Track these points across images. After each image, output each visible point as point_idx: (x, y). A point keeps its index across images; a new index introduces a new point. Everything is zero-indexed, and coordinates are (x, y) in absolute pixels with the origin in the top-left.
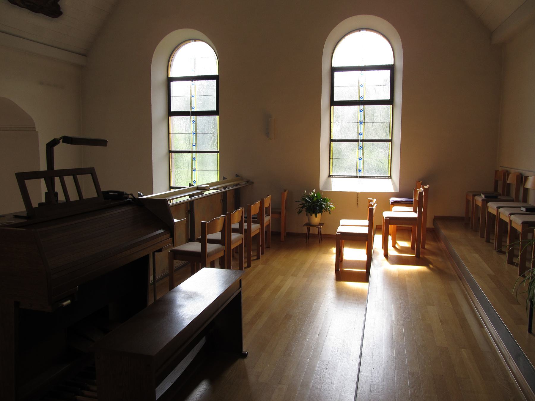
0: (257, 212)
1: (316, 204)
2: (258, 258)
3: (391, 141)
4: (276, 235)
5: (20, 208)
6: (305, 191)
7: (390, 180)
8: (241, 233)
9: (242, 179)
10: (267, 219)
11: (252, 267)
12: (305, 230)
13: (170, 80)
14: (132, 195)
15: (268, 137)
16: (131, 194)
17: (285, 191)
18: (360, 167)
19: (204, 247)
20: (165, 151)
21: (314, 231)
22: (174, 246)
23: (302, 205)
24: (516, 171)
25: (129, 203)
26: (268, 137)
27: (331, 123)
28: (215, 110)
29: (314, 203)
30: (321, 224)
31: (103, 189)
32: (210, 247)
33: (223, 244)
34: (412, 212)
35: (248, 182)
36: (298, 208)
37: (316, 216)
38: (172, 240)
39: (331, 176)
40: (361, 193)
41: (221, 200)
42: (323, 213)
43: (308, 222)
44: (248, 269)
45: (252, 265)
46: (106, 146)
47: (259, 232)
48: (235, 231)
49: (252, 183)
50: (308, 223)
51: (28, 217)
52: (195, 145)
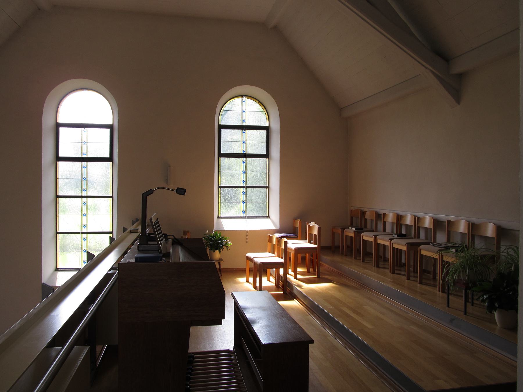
3: (268, 187)
6: (208, 231)
7: (269, 219)
13: (58, 126)
18: (85, 223)
20: (53, 196)
24: (371, 209)
27: (218, 172)
28: (109, 157)
29: (216, 240)
30: (221, 260)
34: (307, 243)
40: (250, 231)
52: (85, 190)
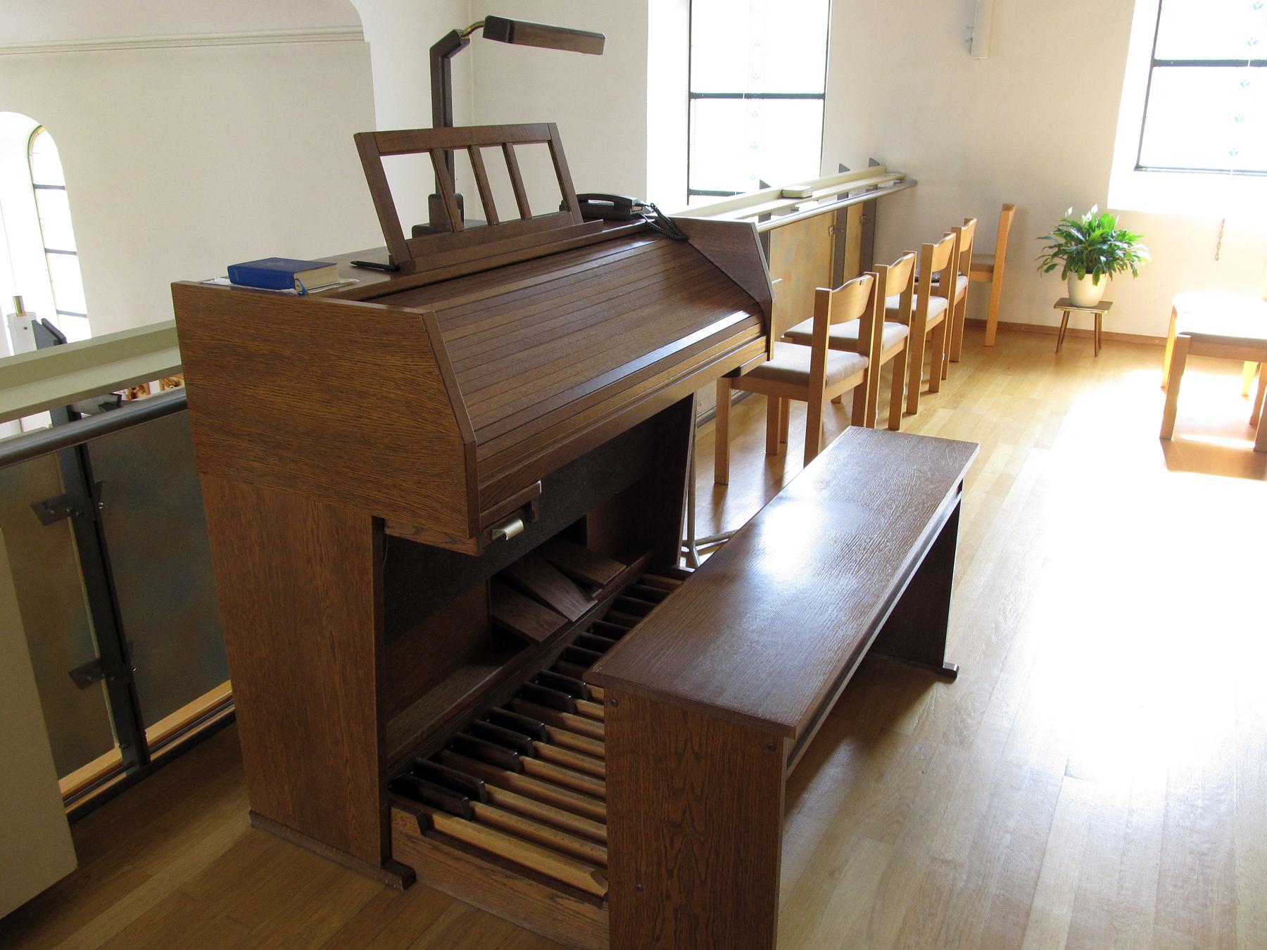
0: (944, 266)
1: (1099, 246)
2: (933, 390)
4: (976, 326)
5: (373, 242)
6: (1070, 211)
8: (904, 322)
9: (886, 172)
10: (962, 283)
11: (920, 415)
12: (1053, 318)
14: (656, 210)
15: (970, 51)
16: (651, 206)
17: (1007, 208)
19: (818, 360)
21: (1082, 321)
22: (768, 360)
23: (1056, 250)
25: (645, 232)
26: (970, 51)
29: (1092, 243)
30: (1104, 305)
31: (580, 188)
32: (835, 361)
33: (865, 353)
35: (901, 180)
36: (1043, 256)
37: (1096, 280)
38: (764, 344)
39: (1141, 167)
41: (831, 229)
42: (1115, 274)
43: (1068, 297)
44: (911, 419)
45: (920, 408)
46: (600, 52)
47: (942, 319)
48: (893, 316)
49: (915, 183)
50: (1064, 299)
51: (393, 269)
